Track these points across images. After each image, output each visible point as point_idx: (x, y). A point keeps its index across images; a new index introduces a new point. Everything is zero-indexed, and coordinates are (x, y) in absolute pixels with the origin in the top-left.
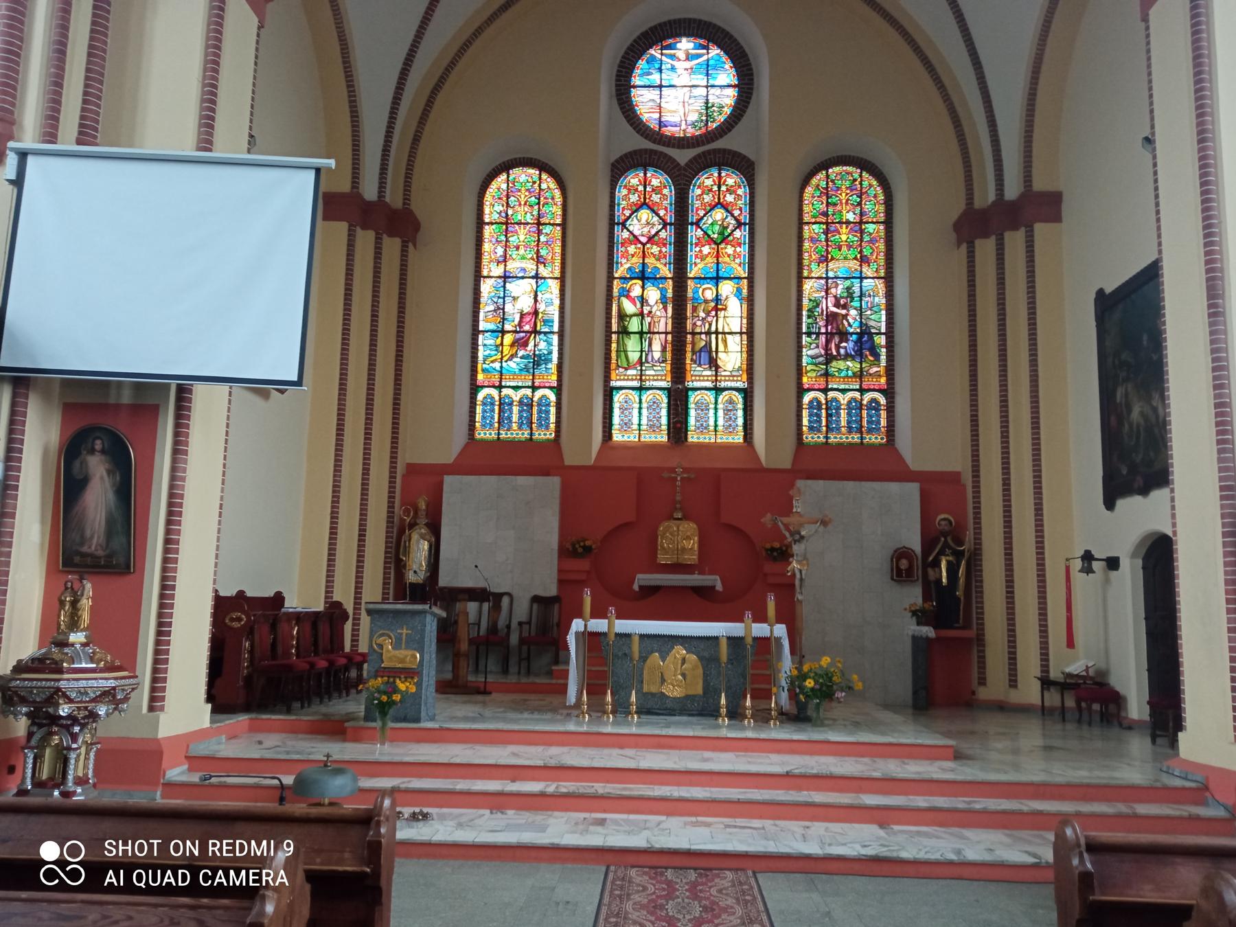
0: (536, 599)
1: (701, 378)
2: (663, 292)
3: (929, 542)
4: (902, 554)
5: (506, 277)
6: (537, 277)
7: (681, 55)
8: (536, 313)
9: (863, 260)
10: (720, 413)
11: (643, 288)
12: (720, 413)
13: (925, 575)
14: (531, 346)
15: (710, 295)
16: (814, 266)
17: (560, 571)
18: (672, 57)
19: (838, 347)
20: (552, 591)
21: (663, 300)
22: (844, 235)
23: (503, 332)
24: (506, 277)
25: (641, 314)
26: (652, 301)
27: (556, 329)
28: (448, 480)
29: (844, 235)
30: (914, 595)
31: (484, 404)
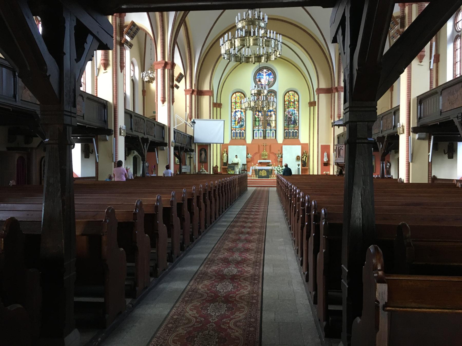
0: (243, 164)
1: (268, 128)
2: (262, 114)
3: (302, 155)
4: (298, 156)
5: (236, 112)
6: (241, 111)
7: (264, 72)
8: (241, 117)
9: (295, 108)
10: (271, 134)
11: (259, 113)
12: (271, 134)
13: (302, 159)
14: (240, 123)
15: (270, 114)
16: (286, 109)
17: (247, 160)
18: (263, 73)
19: (290, 123)
20: (245, 163)
21: (262, 115)
22: (292, 104)
23: (236, 121)
24: (236, 112)
25: (258, 118)
26: (260, 115)
27: (244, 120)
28: (229, 147)
29: (292, 104)
30: (300, 163)
31: (233, 133)
